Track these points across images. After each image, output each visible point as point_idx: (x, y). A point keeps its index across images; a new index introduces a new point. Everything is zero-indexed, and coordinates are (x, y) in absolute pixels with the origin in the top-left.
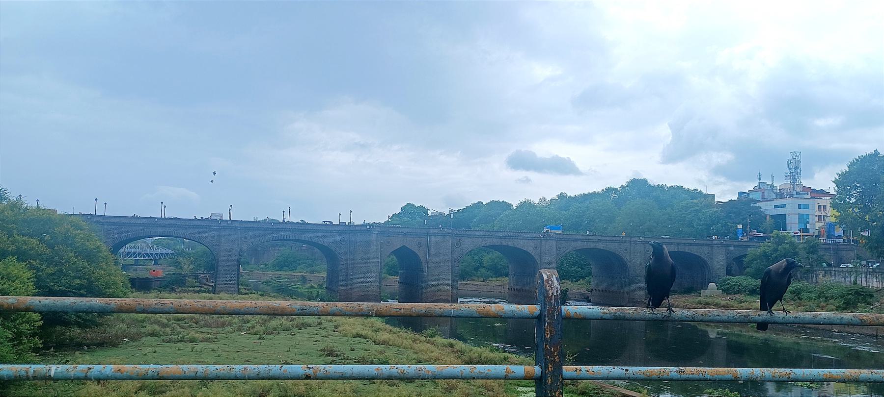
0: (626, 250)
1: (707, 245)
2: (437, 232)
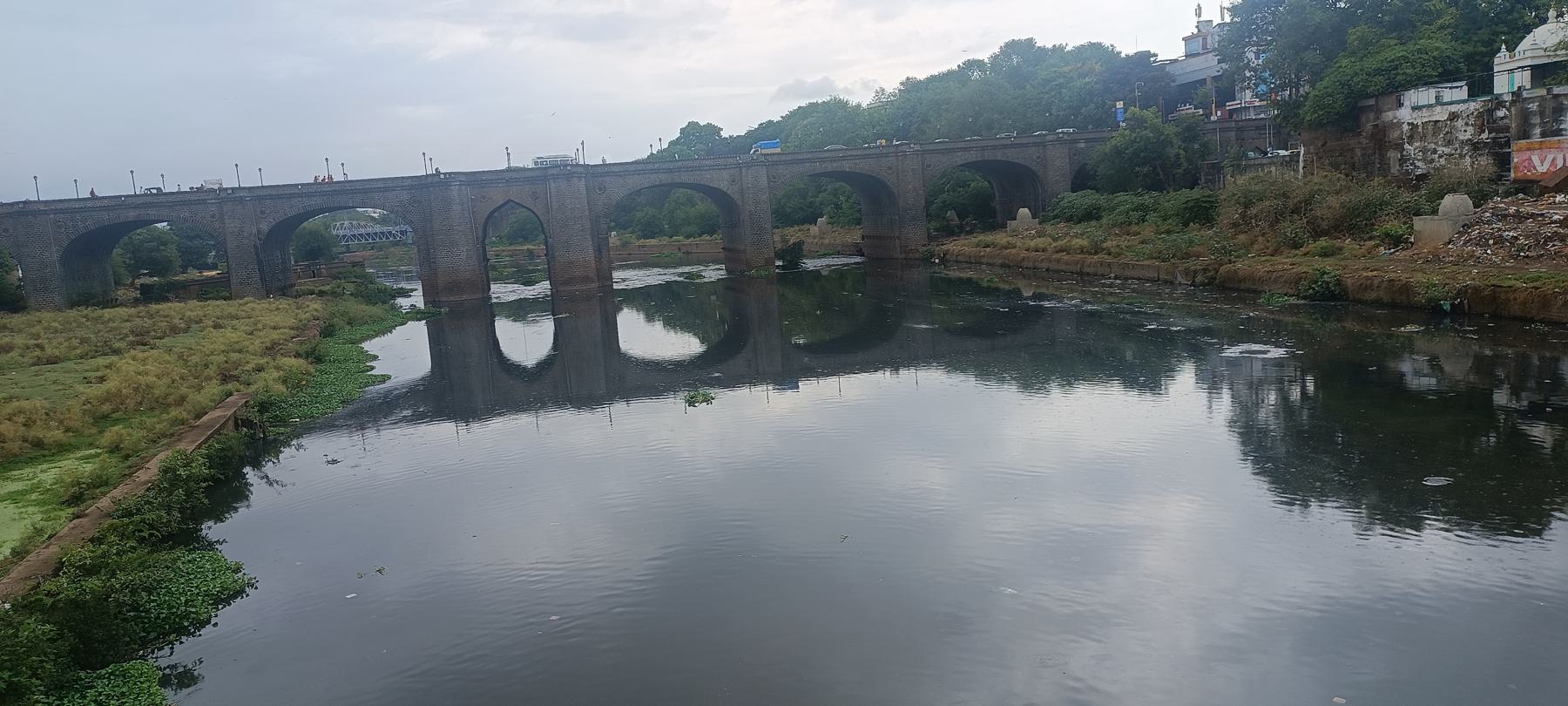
0: (890, 168)
1: (1036, 144)
2: (555, 173)
